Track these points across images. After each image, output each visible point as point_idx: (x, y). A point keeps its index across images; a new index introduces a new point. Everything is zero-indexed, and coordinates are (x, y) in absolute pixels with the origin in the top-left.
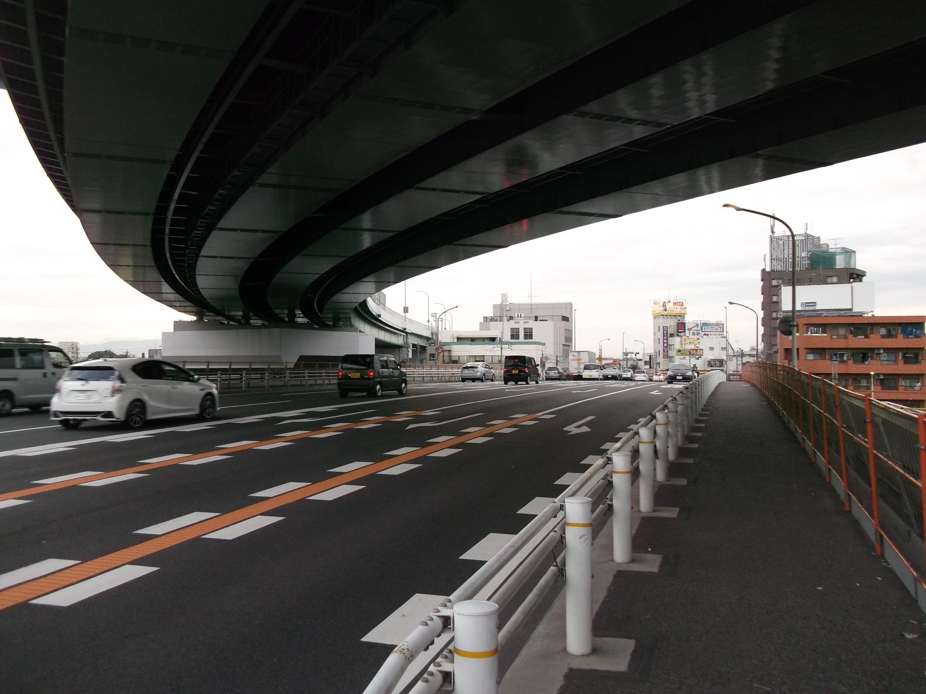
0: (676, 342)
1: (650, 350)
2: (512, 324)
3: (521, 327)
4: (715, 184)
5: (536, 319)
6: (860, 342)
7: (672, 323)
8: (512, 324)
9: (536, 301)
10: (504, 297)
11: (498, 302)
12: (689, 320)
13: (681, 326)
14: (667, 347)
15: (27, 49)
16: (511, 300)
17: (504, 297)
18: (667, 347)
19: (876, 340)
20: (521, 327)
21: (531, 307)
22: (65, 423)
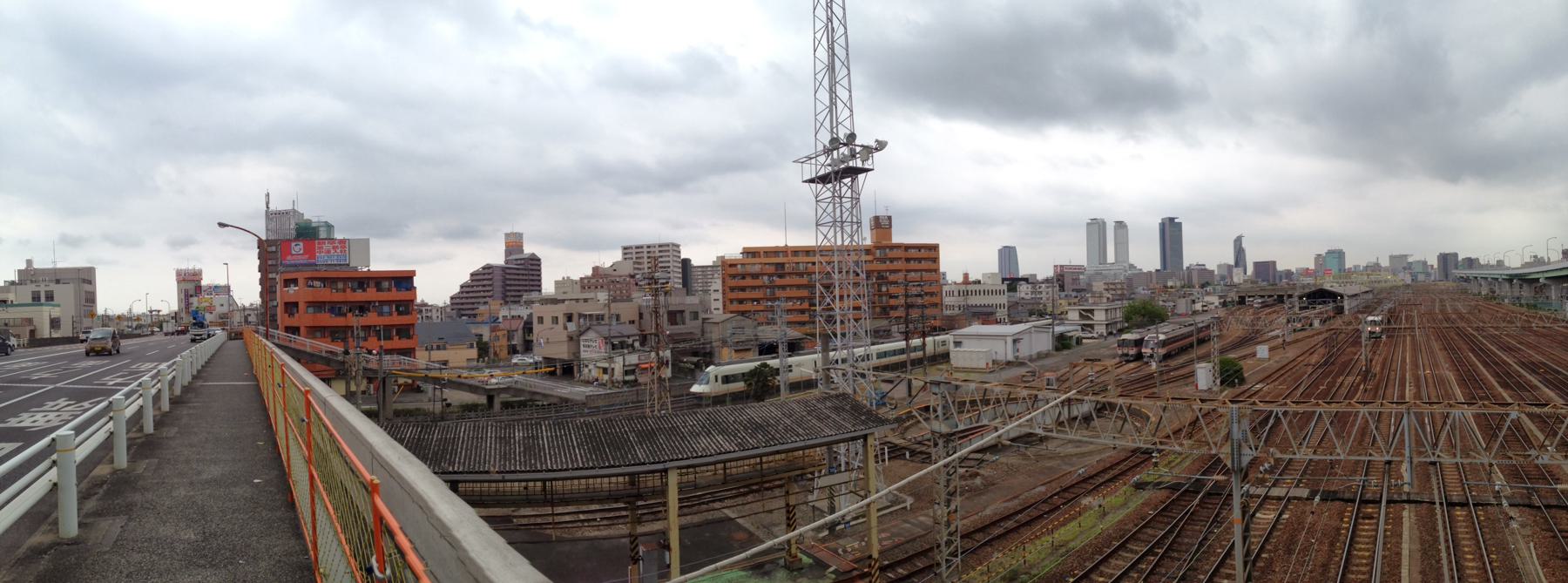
0: (194, 300)
1: (175, 307)
2: (33, 287)
3: (42, 289)
4: (498, 277)
5: (58, 282)
6: (360, 296)
7: (191, 286)
8: (33, 287)
9: (60, 265)
10: (29, 262)
11: (23, 266)
12: (204, 283)
13: (199, 288)
14: (188, 305)
15: (674, 558)
16: (36, 266)
17: (29, 262)
18: (188, 305)
19: (371, 294)
20: (42, 289)
21: (55, 271)
22: (1309, 296)
